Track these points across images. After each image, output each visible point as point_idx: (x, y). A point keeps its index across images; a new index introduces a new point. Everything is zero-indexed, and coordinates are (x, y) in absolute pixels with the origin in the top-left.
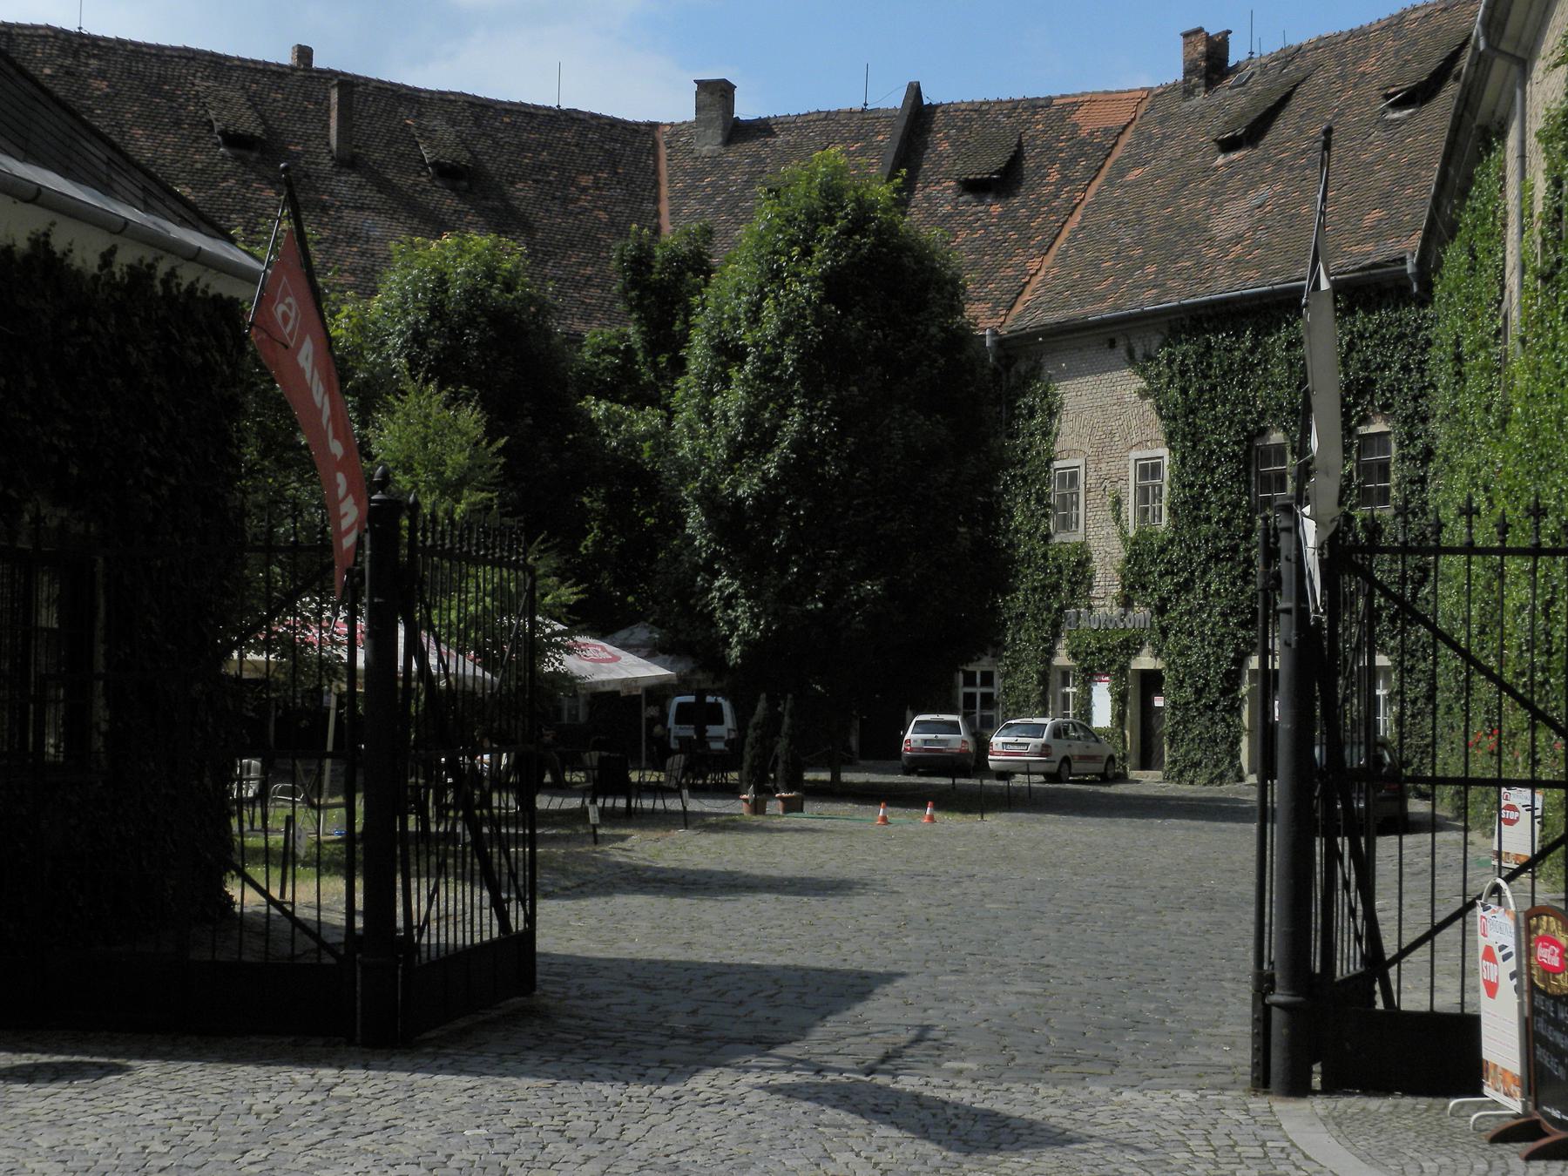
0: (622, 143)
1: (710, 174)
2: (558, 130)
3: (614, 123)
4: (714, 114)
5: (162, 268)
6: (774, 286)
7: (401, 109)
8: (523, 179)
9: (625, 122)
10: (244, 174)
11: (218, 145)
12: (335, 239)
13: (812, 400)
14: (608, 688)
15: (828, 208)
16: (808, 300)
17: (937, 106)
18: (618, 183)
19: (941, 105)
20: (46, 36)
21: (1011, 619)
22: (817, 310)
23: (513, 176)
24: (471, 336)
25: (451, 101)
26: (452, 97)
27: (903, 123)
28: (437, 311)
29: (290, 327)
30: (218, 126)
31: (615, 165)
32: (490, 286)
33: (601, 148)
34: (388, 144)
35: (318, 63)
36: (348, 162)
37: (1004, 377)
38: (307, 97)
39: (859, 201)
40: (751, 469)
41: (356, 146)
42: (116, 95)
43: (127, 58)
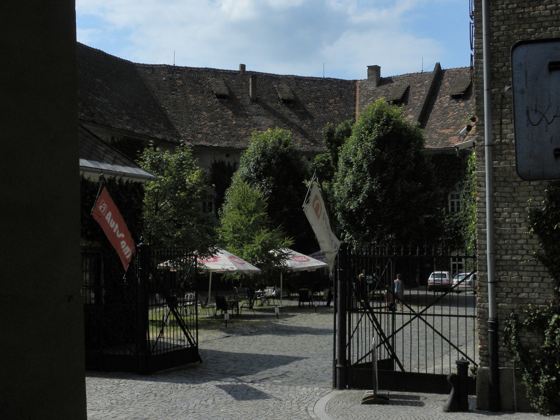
0: (344, 87)
1: (372, 96)
2: (323, 85)
3: (342, 81)
4: (373, 77)
5: (118, 178)
6: (361, 143)
7: (273, 82)
8: (311, 102)
9: (346, 81)
10: (222, 107)
11: (215, 98)
12: (250, 126)
13: (373, 178)
14: (303, 270)
15: (379, 118)
16: (370, 147)
17: (445, 70)
18: (342, 101)
19: (447, 70)
20: (164, 68)
21: (466, 239)
22: (373, 150)
23: (308, 101)
24: (273, 161)
25: (289, 78)
26: (289, 77)
27: (433, 77)
28: (264, 154)
29: (103, 211)
30: (215, 92)
31: (341, 95)
32: (280, 146)
33: (337, 90)
34: (268, 93)
35: (247, 69)
36: (255, 100)
37: (463, 160)
38: (243, 80)
39: (388, 115)
40: (355, 200)
41: (258, 95)
42: (185, 84)
43: (188, 72)
